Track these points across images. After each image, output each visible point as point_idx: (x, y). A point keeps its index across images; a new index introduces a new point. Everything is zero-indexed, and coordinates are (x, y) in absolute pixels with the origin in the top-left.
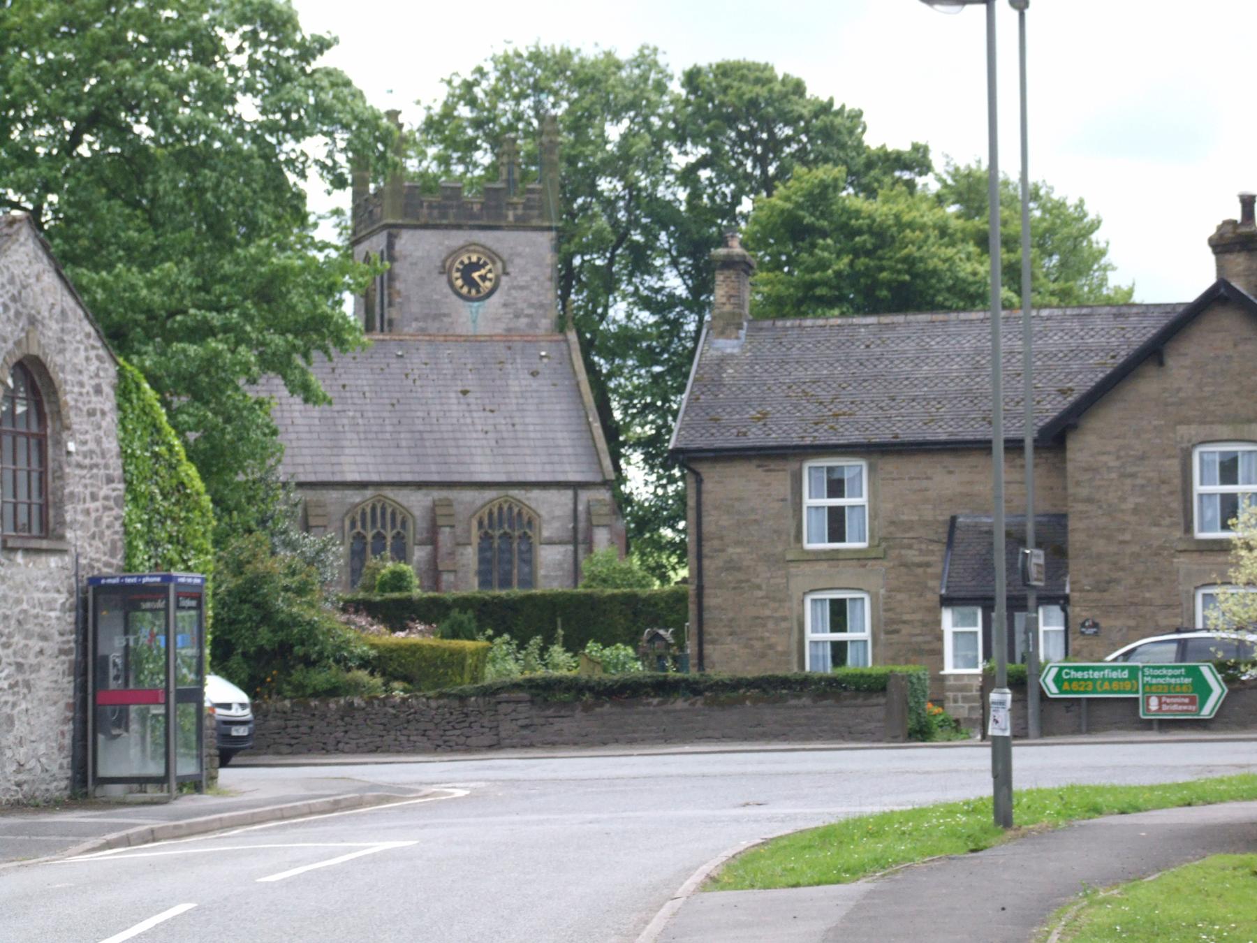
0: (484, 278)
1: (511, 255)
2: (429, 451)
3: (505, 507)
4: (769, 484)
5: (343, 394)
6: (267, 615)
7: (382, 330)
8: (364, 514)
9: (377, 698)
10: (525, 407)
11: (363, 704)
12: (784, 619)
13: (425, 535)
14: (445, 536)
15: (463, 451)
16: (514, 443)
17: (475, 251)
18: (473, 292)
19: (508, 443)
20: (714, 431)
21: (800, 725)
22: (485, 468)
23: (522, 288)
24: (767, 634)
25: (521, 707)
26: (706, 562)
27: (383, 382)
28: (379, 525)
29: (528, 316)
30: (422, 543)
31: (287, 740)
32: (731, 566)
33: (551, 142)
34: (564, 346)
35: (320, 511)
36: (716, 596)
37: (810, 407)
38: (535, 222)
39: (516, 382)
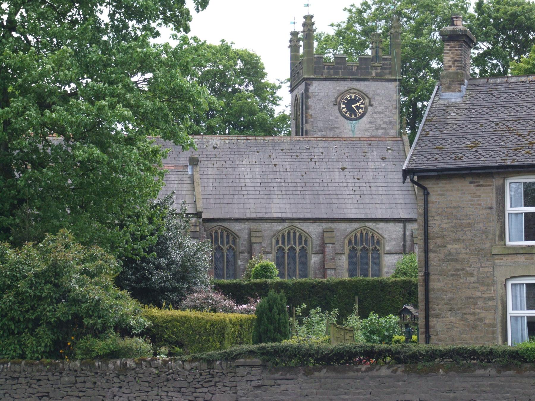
0: (358, 108)
1: (373, 95)
2: (322, 201)
3: (364, 233)
4: (479, 196)
5: (275, 170)
6: (64, 294)
7: (302, 135)
8: (283, 237)
9: (145, 360)
10: (377, 177)
11: (134, 365)
12: (491, 299)
13: (318, 248)
14: (329, 250)
15: (341, 201)
16: (370, 197)
17: (353, 93)
18: (353, 115)
19: (367, 197)
20: (438, 156)
21: (485, 392)
22: (353, 211)
23: (380, 113)
24: (478, 311)
25: (254, 371)
26: (431, 256)
27: (297, 163)
28: (303, 243)
29: (383, 128)
30: (316, 253)
31: (76, 393)
32: (451, 258)
33: (396, 32)
34: (401, 144)
35: (258, 234)
36: (439, 281)
37: (512, 138)
38: (387, 77)
39: (373, 163)
